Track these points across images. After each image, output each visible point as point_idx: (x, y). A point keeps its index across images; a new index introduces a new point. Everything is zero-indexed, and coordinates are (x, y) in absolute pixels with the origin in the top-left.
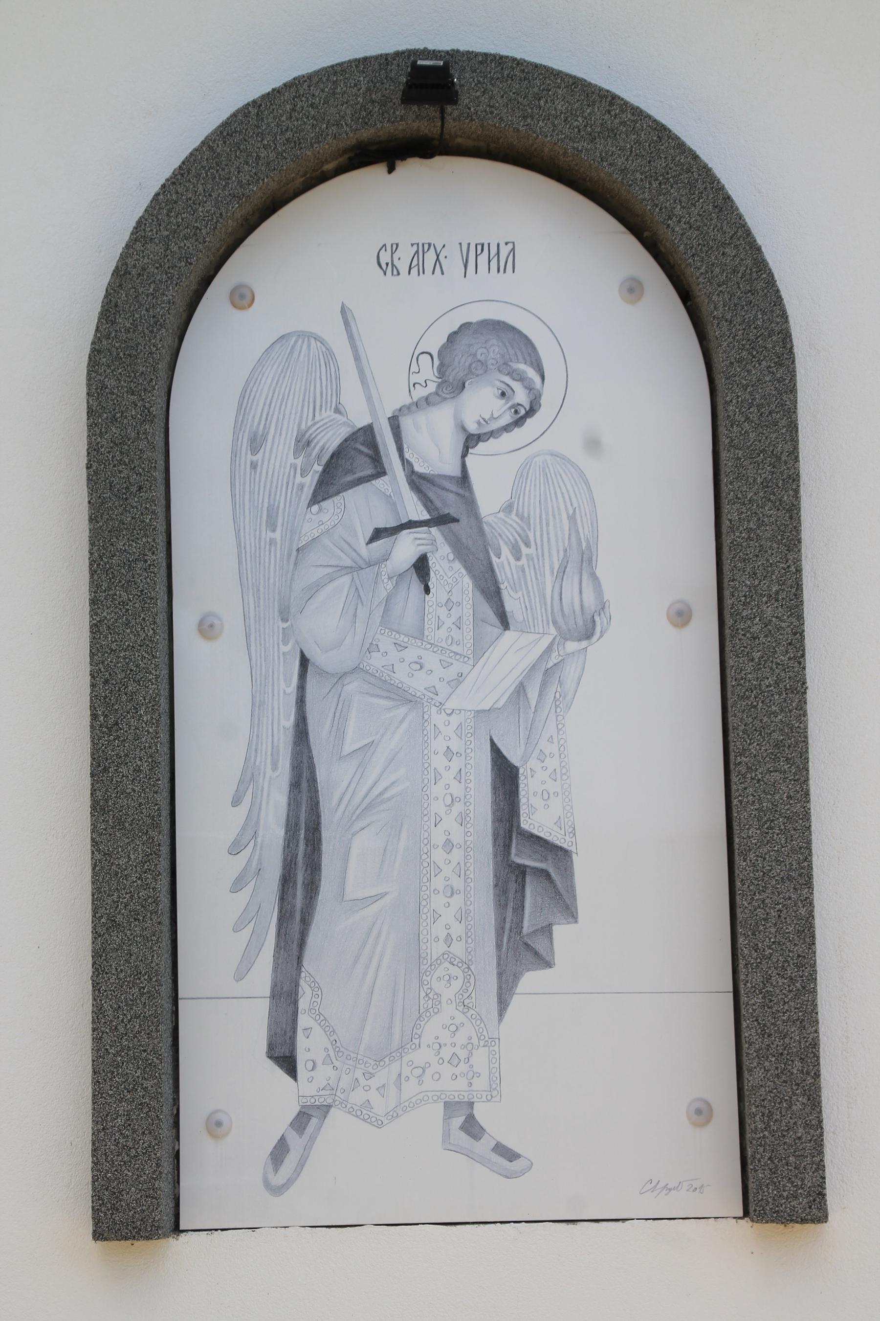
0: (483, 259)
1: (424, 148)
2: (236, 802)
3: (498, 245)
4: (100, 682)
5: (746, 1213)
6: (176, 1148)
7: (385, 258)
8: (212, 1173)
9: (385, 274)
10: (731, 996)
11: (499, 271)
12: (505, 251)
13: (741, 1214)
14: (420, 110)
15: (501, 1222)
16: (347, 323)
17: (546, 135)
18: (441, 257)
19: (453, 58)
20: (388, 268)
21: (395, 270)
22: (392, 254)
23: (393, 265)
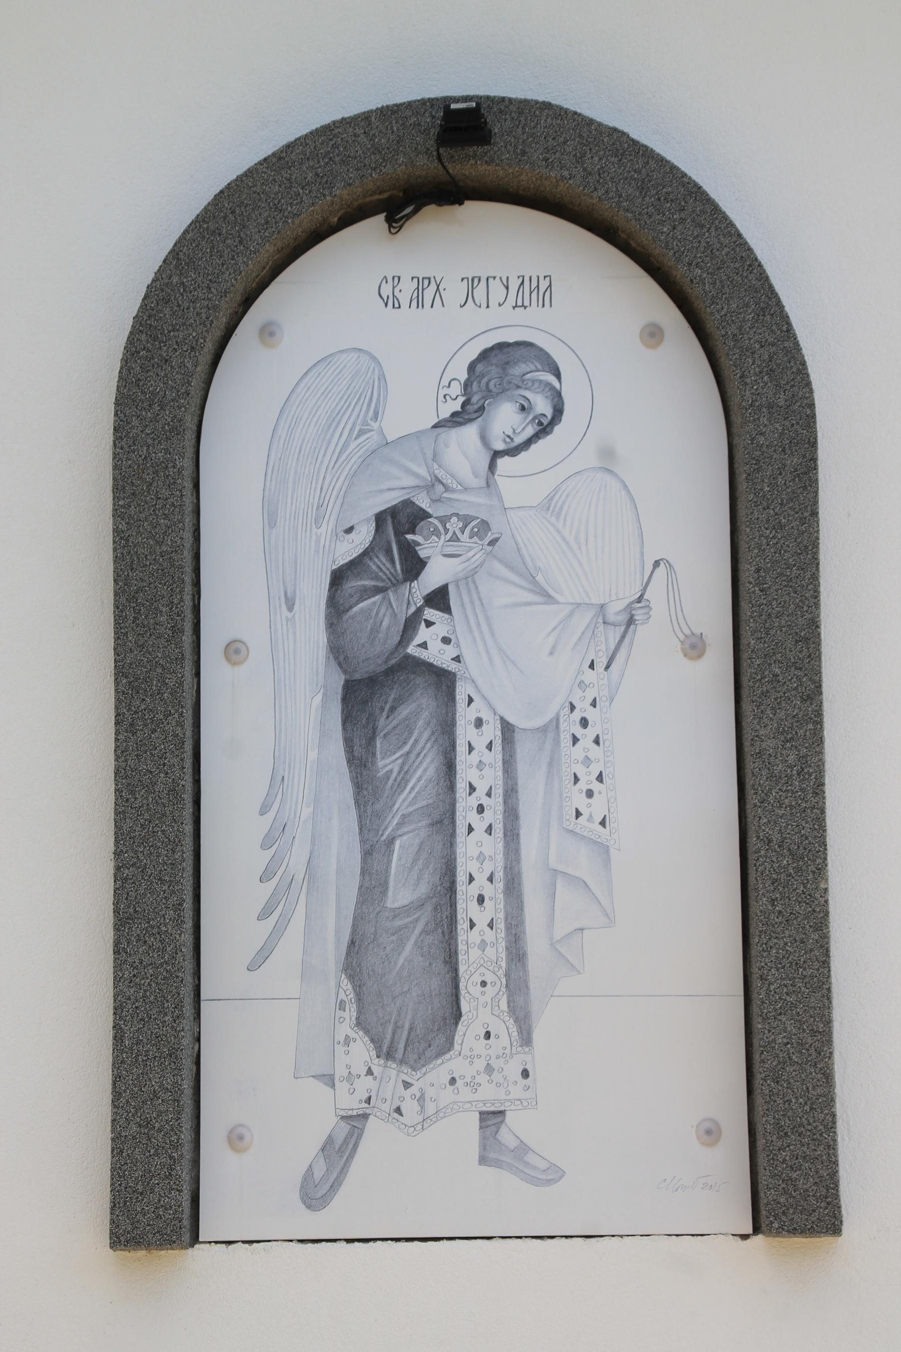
1: (451, 193)
2: (263, 812)
5: (757, 1230)
7: (387, 290)
8: (234, 1184)
9: (386, 305)
12: (544, 285)
13: (749, 1230)
14: (446, 157)
17: (569, 183)
22: (394, 287)
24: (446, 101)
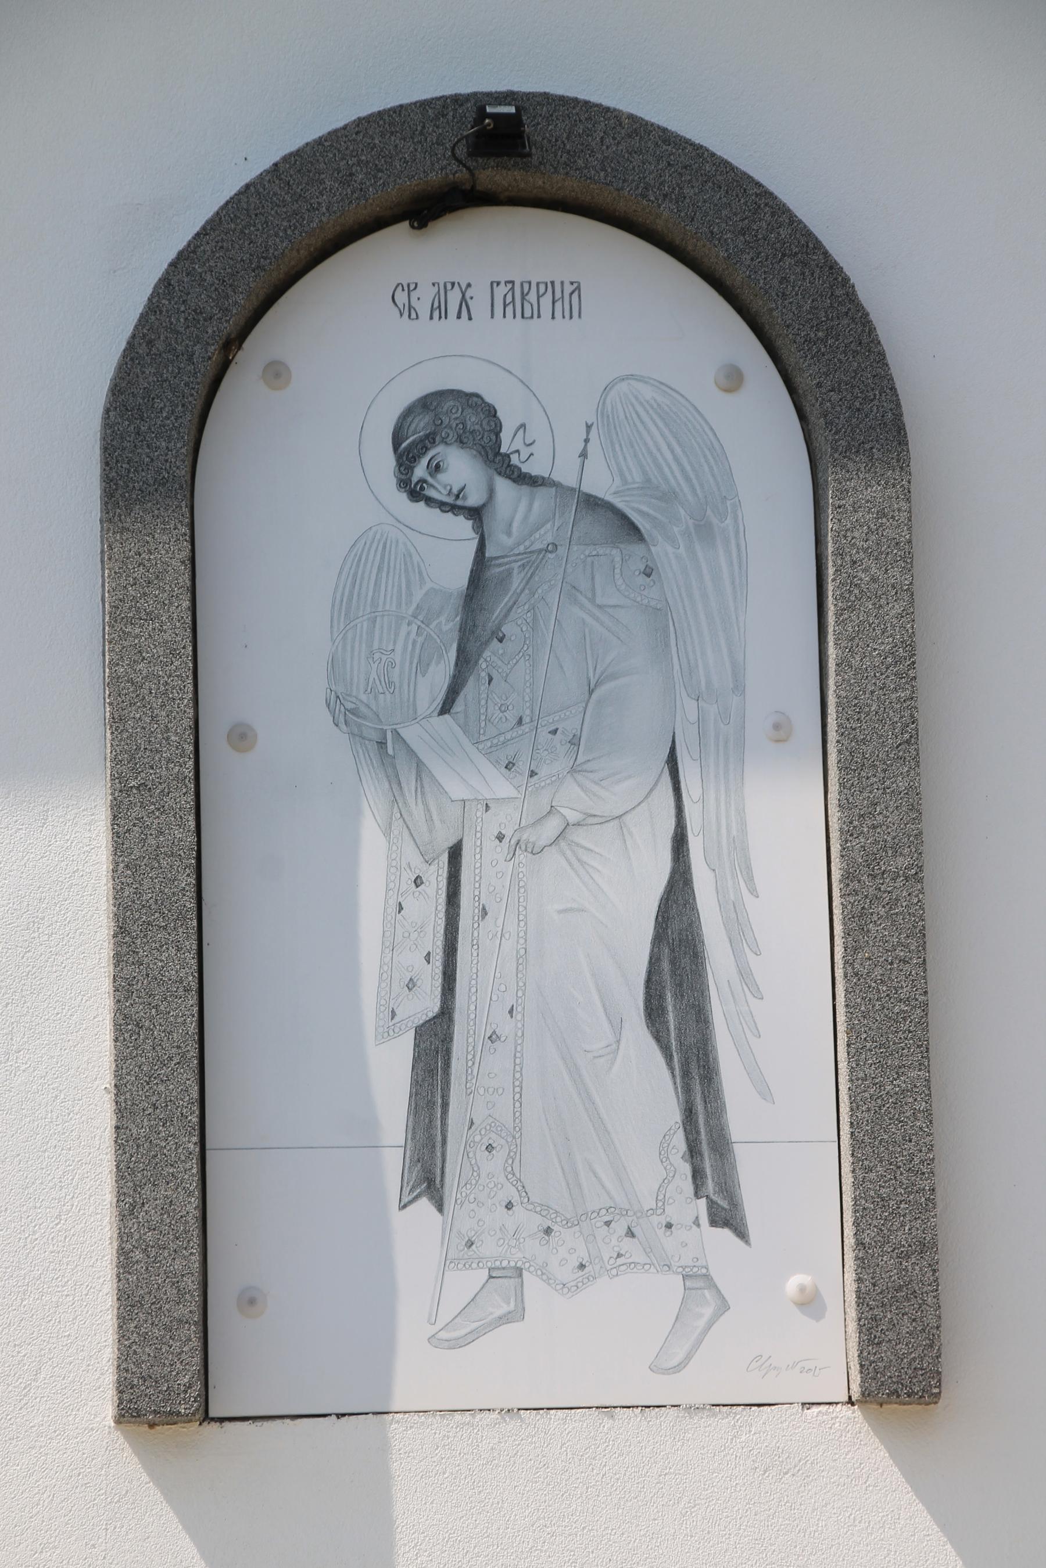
0: (546, 301)
6: (656, 950)
7: (401, 297)
10: (208, 1146)
14: (489, 156)
16: (508, 371)
19: (525, 102)
20: (410, 312)
21: (412, 311)
23: (410, 307)
24: (479, 101)
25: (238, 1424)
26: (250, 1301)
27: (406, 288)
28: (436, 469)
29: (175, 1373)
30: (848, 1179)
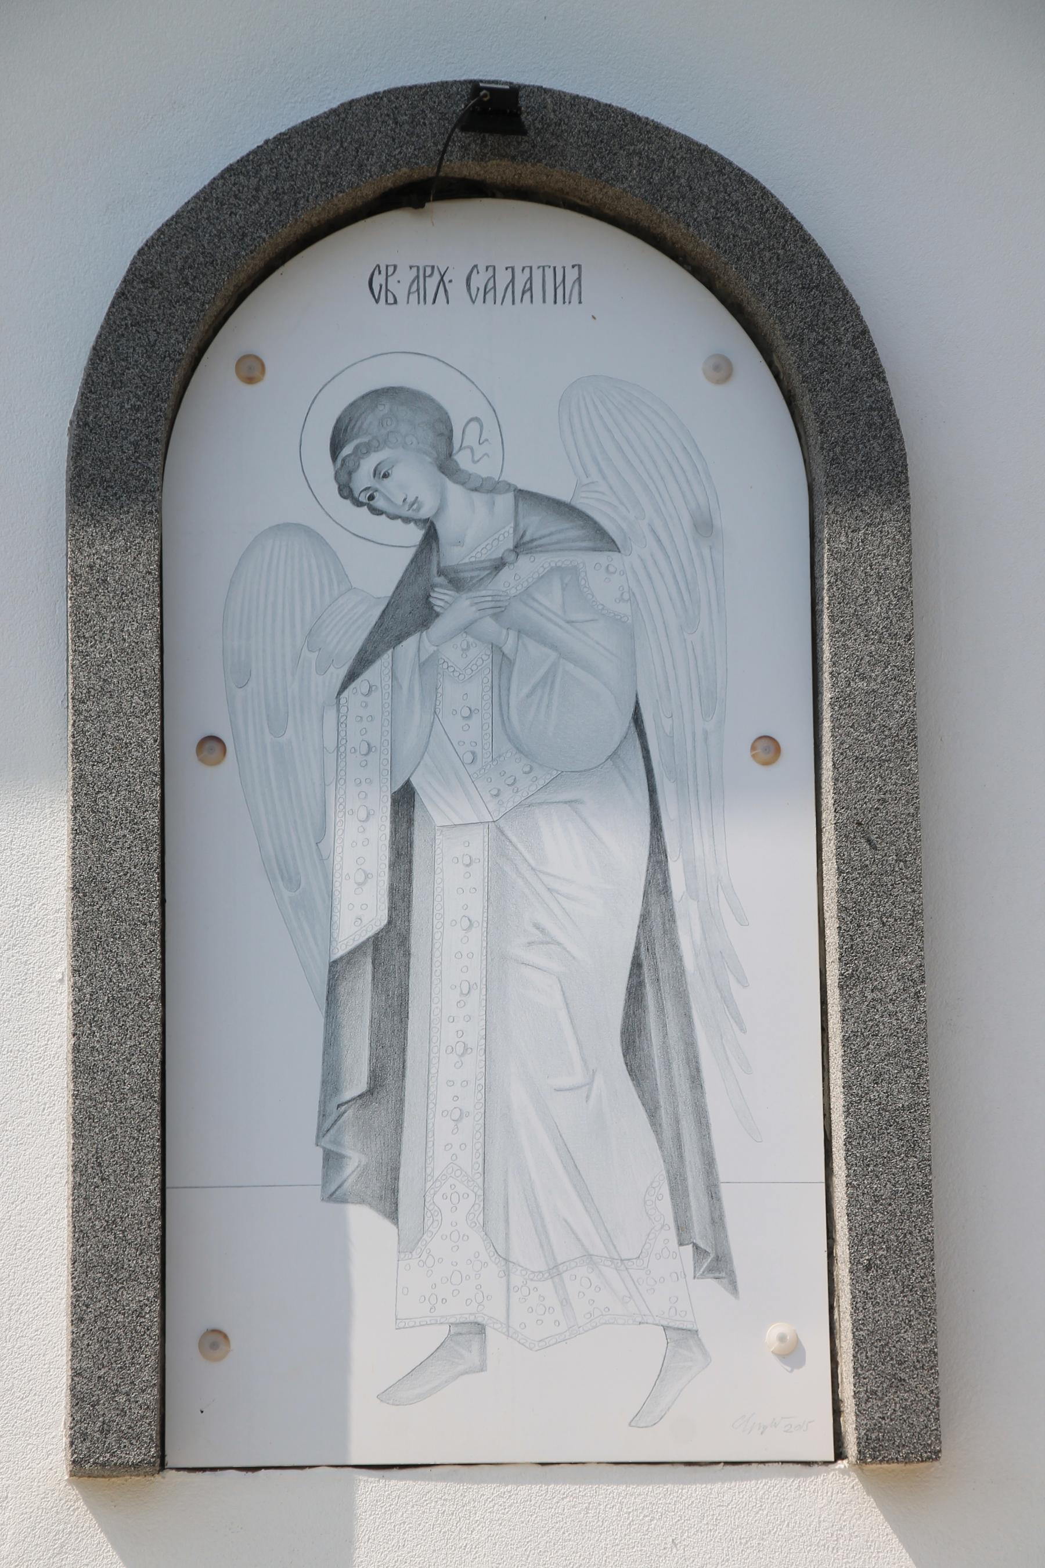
3: (564, 268)
4: (104, 366)
10: (168, 1185)
11: (555, 302)
12: (572, 275)
14: (485, 145)
15: (749, 1463)
18: (446, 279)
24: (475, 87)
25: (200, 1474)
26: (215, 1340)
27: (383, 272)
28: (382, 474)
29: (129, 1424)
30: (831, 883)
